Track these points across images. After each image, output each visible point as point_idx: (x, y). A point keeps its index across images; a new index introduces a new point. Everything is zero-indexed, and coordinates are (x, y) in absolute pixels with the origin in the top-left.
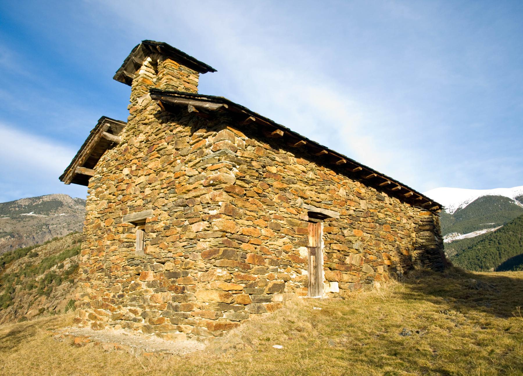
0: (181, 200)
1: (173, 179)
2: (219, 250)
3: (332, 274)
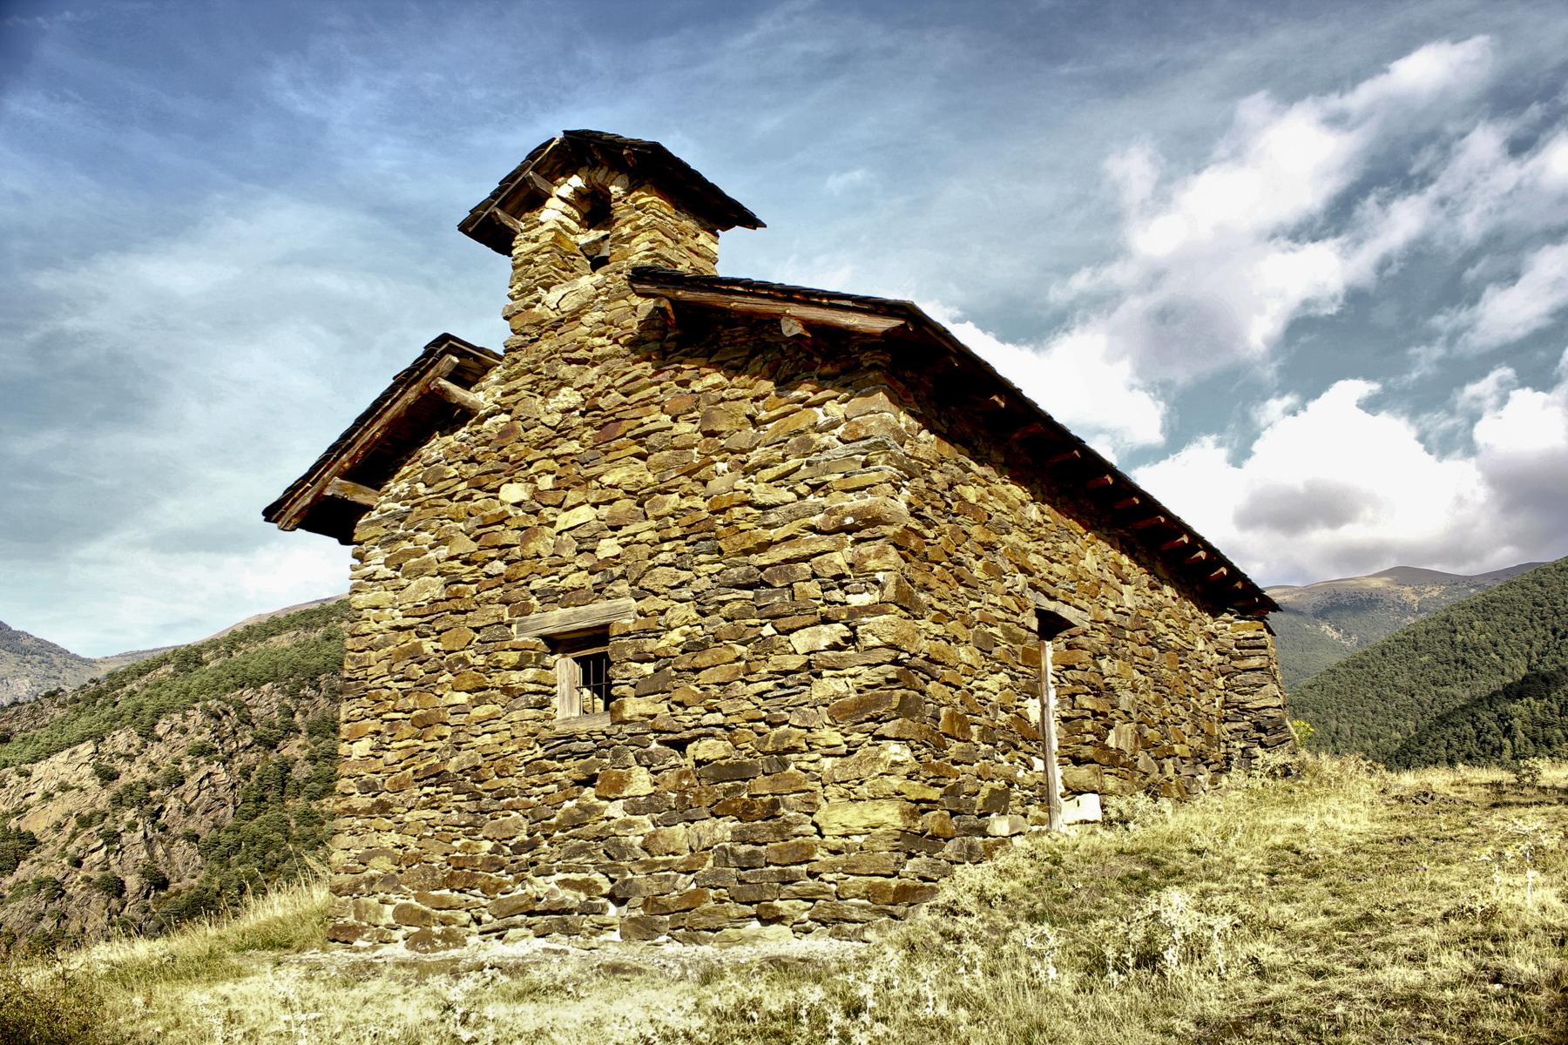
0: (743, 569)
1: (705, 514)
2: (890, 696)
3: (1083, 774)
